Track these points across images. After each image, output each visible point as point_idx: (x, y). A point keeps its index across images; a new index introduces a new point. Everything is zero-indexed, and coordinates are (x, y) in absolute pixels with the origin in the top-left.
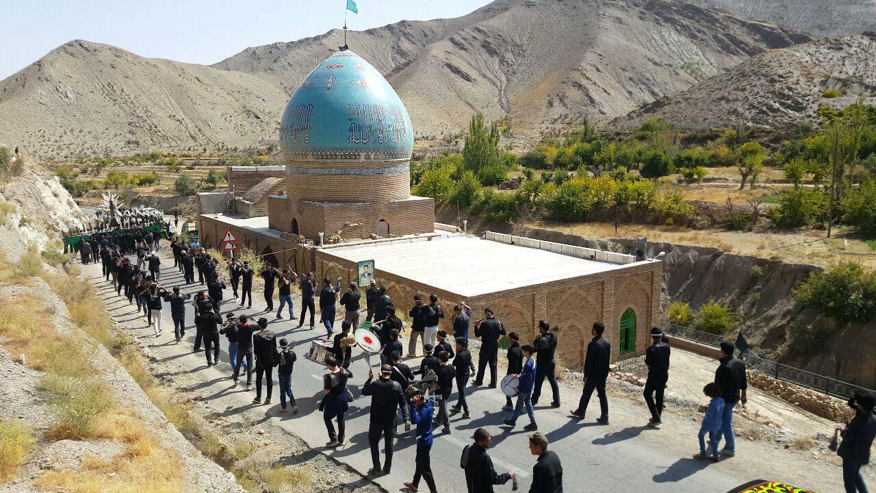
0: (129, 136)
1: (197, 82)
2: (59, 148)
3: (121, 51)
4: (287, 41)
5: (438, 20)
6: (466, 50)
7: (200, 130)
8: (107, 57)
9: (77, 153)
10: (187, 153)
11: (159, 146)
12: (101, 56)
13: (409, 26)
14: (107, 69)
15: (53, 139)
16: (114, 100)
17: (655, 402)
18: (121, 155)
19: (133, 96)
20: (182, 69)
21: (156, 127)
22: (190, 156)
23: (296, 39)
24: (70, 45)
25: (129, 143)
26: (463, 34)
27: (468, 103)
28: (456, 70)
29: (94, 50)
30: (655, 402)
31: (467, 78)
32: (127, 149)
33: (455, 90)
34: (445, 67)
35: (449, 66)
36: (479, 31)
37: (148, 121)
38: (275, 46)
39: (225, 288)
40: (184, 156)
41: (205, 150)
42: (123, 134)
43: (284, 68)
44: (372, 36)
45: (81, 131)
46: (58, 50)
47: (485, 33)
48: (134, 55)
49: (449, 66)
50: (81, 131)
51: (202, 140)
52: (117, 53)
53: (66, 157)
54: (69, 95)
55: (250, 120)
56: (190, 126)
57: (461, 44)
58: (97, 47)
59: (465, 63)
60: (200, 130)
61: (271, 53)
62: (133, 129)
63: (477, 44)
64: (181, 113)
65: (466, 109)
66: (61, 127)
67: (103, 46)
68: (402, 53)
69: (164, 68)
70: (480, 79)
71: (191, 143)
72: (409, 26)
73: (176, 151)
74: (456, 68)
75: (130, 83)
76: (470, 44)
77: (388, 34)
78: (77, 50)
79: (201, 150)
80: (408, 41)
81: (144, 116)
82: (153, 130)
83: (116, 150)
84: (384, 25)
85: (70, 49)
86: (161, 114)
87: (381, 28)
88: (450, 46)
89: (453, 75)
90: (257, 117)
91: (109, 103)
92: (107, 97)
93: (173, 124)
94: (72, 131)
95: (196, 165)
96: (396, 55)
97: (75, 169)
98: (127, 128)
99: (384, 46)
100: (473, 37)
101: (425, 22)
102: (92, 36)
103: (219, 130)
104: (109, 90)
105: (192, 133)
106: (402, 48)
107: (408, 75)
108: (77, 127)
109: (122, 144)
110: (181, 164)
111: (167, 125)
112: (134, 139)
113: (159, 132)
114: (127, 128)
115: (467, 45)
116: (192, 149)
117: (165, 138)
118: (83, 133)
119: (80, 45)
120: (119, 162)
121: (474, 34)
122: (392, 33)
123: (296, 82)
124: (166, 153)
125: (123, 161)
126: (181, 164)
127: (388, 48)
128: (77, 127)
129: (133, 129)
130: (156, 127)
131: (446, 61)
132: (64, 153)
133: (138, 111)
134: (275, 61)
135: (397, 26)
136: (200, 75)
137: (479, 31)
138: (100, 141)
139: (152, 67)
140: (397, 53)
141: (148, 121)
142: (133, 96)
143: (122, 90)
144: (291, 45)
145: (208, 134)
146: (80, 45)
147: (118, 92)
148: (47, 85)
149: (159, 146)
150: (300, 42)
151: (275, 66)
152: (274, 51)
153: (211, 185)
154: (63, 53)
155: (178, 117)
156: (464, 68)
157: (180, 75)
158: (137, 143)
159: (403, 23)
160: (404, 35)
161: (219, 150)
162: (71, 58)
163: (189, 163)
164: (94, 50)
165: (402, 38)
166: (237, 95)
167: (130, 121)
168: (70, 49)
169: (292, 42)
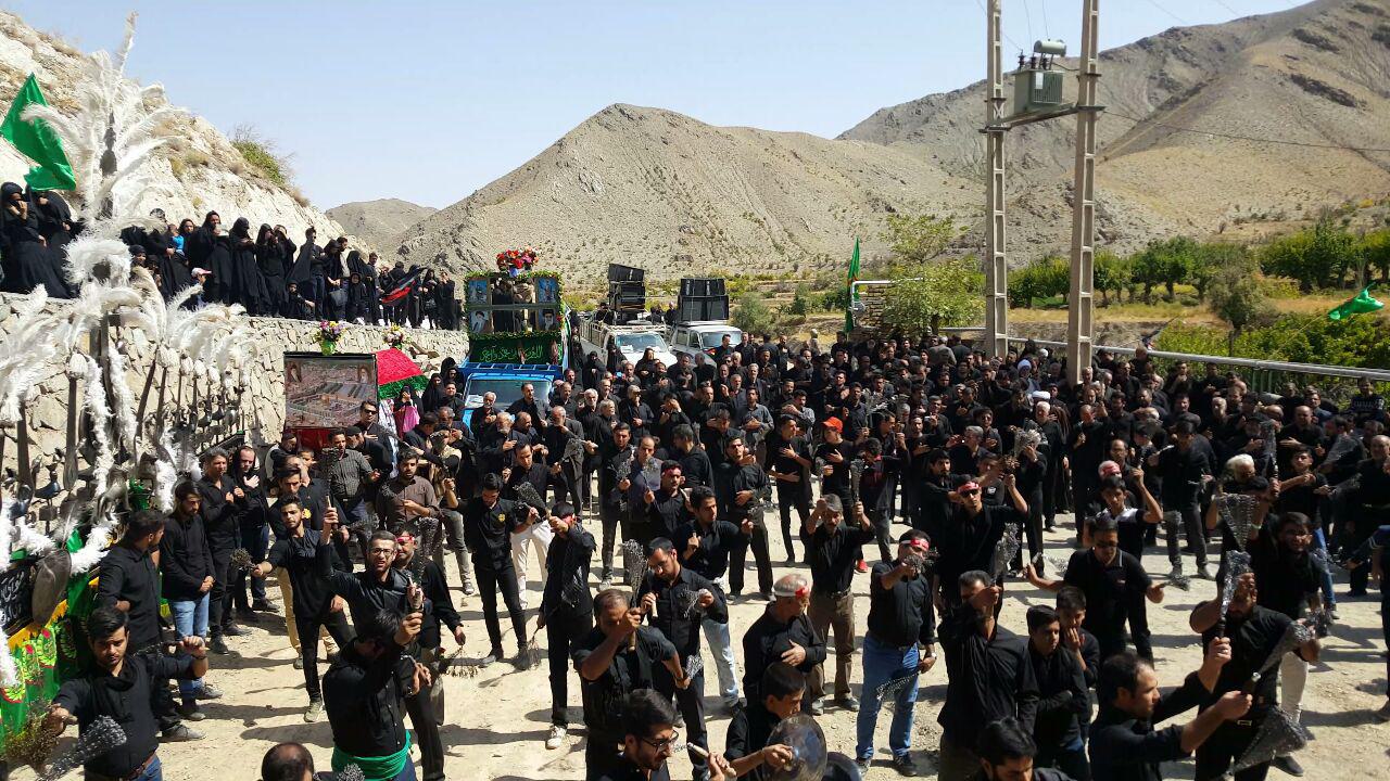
0: (678, 247)
1: (793, 159)
2: (572, 267)
3: (680, 117)
4: (946, 90)
5: (1248, 18)
6: (1334, 49)
7: (790, 235)
8: (657, 127)
9: (597, 276)
10: (765, 274)
11: (722, 262)
12: (648, 126)
13: (1186, 35)
14: (657, 146)
15: (564, 255)
16: (662, 193)
17: (1127, 624)
18: (662, 279)
19: (690, 185)
20: (771, 141)
21: (721, 233)
22: (771, 278)
23: (962, 86)
24: (606, 112)
25: (676, 258)
26: (1326, 20)
27: (1353, 149)
28: (1317, 88)
29: (640, 118)
30: (1127, 624)
31: (1345, 100)
32: (673, 268)
33: (1316, 126)
34: (1289, 84)
35: (1299, 80)
36: (1365, 9)
37: (710, 224)
38: (927, 101)
39: (58, 452)
40: (761, 278)
41: (796, 267)
42: (669, 245)
43: (941, 129)
44: (1108, 62)
45: (607, 242)
46: (588, 123)
47: (1380, 13)
48: (698, 122)
49: (1299, 80)
50: (607, 242)
51: (792, 251)
52: (673, 120)
53: (579, 283)
54: (596, 186)
55: (877, 215)
56: (775, 229)
57: (1322, 39)
58: (645, 114)
59: (1335, 76)
60: (790, 235)
61: (918, 112)
62: (685, 236)
63: (1362, 37)
64: (762, 209)
65: (1348, 159)
66: (579, 236)
67: (653, 111)
68: (1166, 83)
69: (743, 140)
70: (1374, 100)
71: (775, 257)
72: (1186, 35)
73: (748, 270)
74: (1316, 83)
75: (689, 164)
76: (1344, 37)
77: (1142, 55)
78: (617, 118)
79: (789, 267)
80: (1181, 62)
81: (705, 217)
82: (717, 236)
83: (655, 271)
84: (1133, 40)
85: (606, 119)
86: (731, 212)
87: (1128, 47)
88: (1295, 46)
89: (1308, 97)
90: (890, 210)
91: (654, 198)
92: (651, 189)
93: (746, 226)
94: (594, 240)
95: (777, 290)
96: (1158, 91)
97: (590, 300)
98: (676, 236)
99: (1132, 76)
100: (1351, 23)
101: (1220, 26)
102: (636, 99)
103: (821, 233)
104: (656, 178)
105: (778, 241)
106: (1171, 76)
107: (1201, 108)
108: (601, 234)
109: (666, 261)
110: (755, 289)
111: (738, 229)
112: (684, 252)
113: (726, 240)
114: (676, 236)
115: (1334, 40)
116: (775, 266)
117: (734, 250)
118: (610, 245)
119: (621, 110)
120: (658, 289)
121: (1353, 18)
122: (1150, 52)
123: (962, 150)
124: (732, 274)
125: (664, 287)
126: (755, 289)
127: (1142, 79)
128: (601, 234)
129: (685, 236)
130: (721, 233)
131: (1289, 73)
132: (578, 276)
133: (695, 209)
134: (927, 121)
135: (1159, 39)
136: (802, 148)
137: (1365, 9)
138: (633, 257)
139: (722, 140)
140: (1159, 86)
141: (710, 224)
142: (690, 185)
143: (675, 176)
144: (953, 97)
145: (804, 240)
146: (621, 110)
147: (668, 181)
148: (567, 174)
149: (722, 262)
150: (969, 88)
151: (925, 129)
152: (925, 110)
153: (797, 317)
154: (595, 126)
155: (757, 216)
156: (1333, 81)
157: (766, 150)
158: (689, 259)
159: (1173, 32)
160: (1174, 53)
161: (820, 266)
162: (605, 131)
163: (766, 289)
164: (640, 118)
165: (1171, 58)
166: (857, 177)
167: (682, 224)
168: (606, 119)
169: (957, 91)
